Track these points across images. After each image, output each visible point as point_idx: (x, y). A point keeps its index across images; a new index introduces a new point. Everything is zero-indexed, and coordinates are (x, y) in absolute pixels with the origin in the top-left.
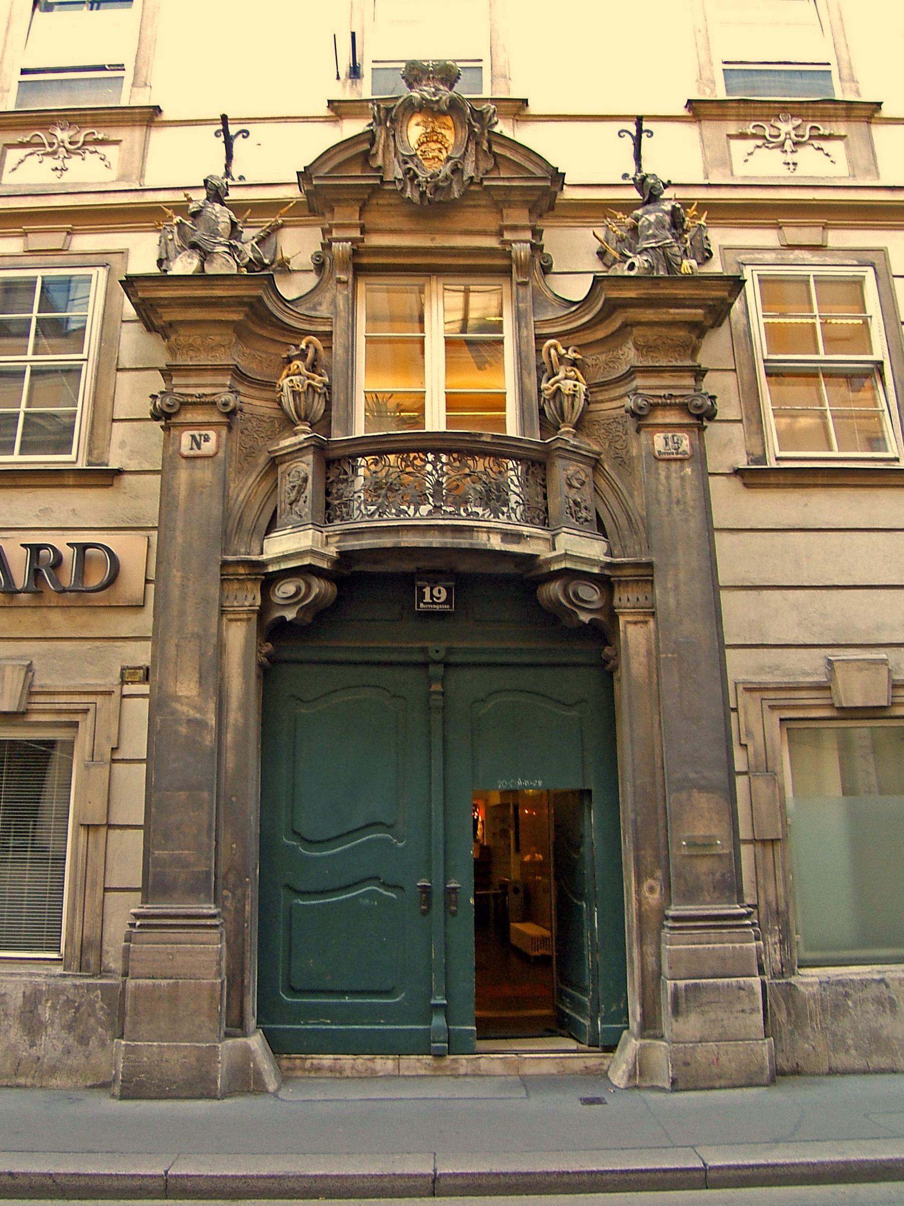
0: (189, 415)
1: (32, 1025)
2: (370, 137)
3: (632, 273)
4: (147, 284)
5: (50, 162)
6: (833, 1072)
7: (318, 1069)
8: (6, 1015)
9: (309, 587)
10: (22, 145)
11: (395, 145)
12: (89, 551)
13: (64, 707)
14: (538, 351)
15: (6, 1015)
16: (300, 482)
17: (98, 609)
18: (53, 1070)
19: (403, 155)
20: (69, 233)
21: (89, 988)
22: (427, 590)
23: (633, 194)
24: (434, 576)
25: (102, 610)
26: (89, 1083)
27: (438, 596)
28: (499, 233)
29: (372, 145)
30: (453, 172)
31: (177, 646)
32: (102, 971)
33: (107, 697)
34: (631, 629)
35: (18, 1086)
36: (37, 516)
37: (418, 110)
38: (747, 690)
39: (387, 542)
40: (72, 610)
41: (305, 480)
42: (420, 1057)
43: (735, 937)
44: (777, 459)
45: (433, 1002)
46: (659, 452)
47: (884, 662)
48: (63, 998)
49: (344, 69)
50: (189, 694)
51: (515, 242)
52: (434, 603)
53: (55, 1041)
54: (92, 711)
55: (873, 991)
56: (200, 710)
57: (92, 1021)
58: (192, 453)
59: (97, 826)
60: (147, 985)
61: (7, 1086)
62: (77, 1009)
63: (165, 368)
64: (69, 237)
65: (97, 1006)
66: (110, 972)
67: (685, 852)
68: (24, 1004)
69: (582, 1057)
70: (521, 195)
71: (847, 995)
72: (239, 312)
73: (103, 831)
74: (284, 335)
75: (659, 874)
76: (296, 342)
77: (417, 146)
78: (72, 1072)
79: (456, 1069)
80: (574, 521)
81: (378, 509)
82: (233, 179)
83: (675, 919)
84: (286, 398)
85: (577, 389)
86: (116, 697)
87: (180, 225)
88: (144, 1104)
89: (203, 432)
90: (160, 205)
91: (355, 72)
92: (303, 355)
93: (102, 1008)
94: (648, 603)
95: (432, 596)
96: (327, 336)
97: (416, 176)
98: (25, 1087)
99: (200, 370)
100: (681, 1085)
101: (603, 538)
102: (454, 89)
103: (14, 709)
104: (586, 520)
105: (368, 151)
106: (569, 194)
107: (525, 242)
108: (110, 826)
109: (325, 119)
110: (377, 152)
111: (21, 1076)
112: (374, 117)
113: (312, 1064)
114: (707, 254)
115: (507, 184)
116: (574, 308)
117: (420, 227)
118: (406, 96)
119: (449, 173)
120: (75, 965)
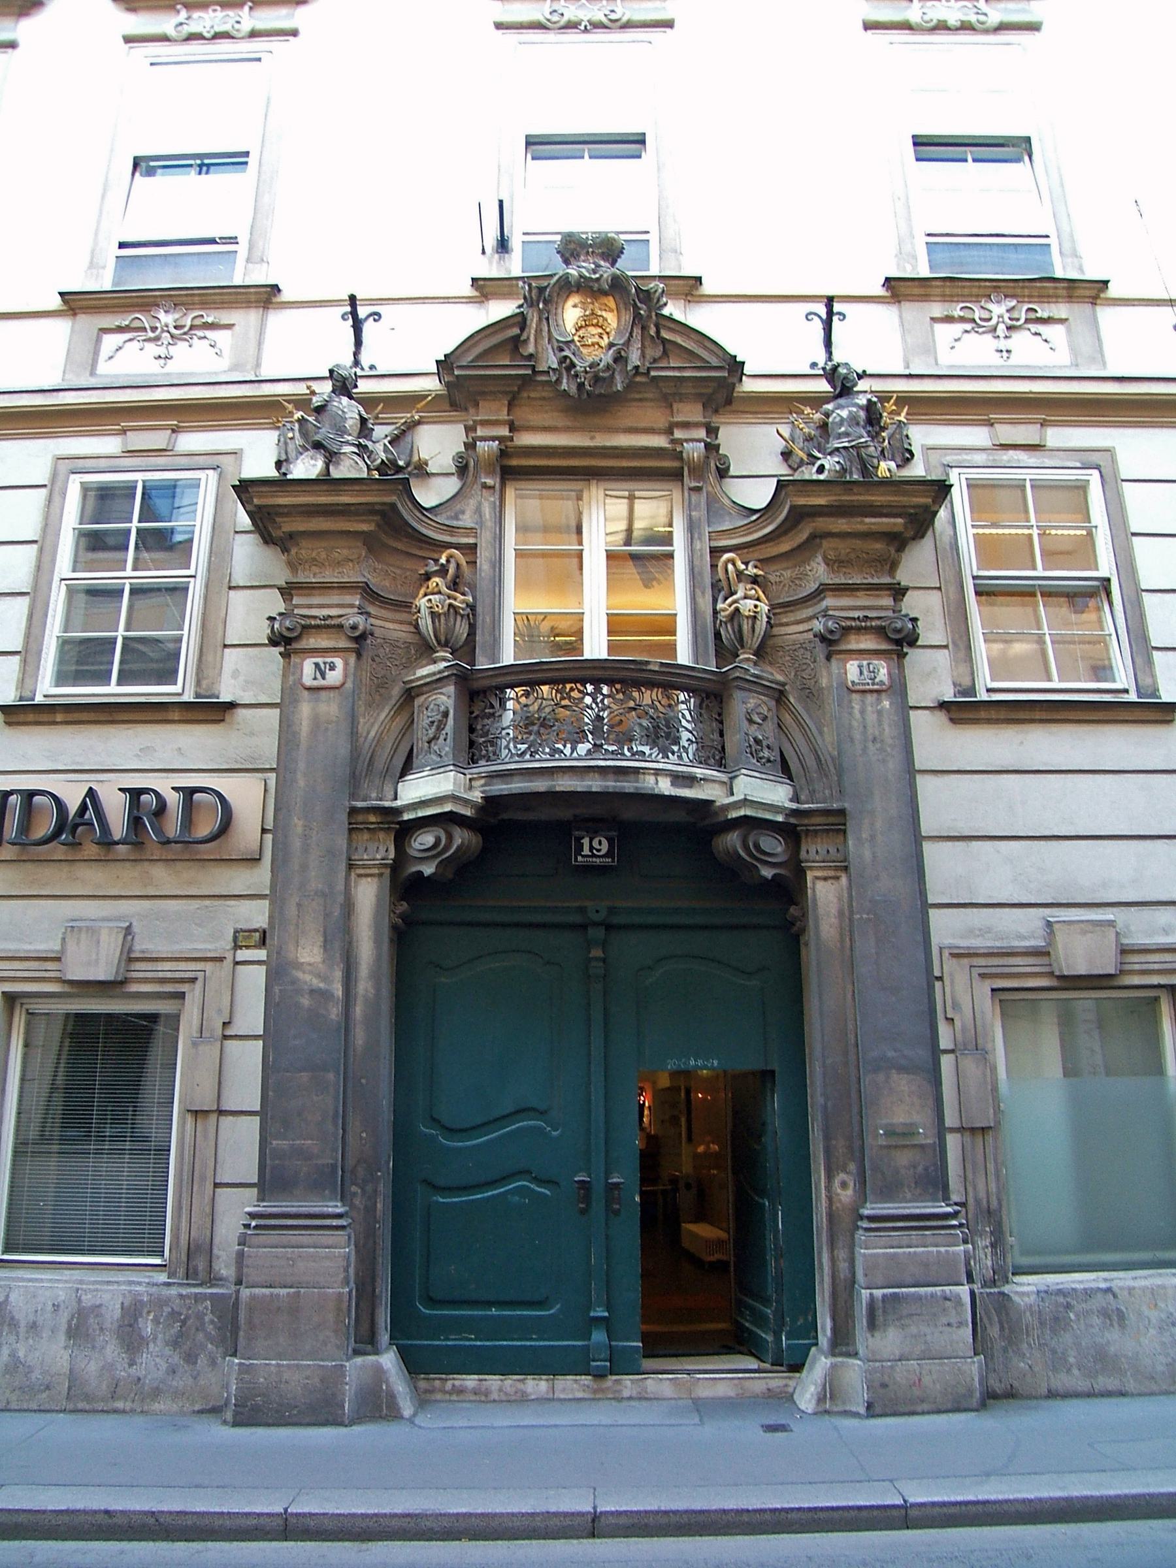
0: (312, 641)
1: (131, 1339)
2: (520, 320)
3: (822, 477)
4: (264, 489)
5: (152, 349)
6: (1052, 1395)
7: (461, 1391)
8: (101, 1329)
9: (450, 837)
10: (120, 329)
11: (549, 330)
12: (197, 796)
13: (169, 975)
15: (101, 1329)
16: (439, 717)
17: (207, 863)
18: (156, 1393)
19: (558, 341)
20: (174, 431)
21: (198, 1298)
22: (586, 842)
23: (823, 386)
24: (594, 825)
25: (212, 863)
26: (196, 1408)
28: (669, 431)
30: (616, 360)
31: (299, 905)
32: (212, 1279)
33: (218, 964)
34: (820, 885)
35: (116, 1411)
36: (137, 756)
38: (953, 955)
39: (540, 785)
40: (178, 863)
41: (446, 714)
42: (578, 1377)
43: (940, 1239)
44: (988, 690)
45: (592, 1314)
46: (853, 682)
47: (1111, 923)
48: (167, 1310)
49: (491, 242)
50: (313, 960)
51: (687, 441)
52: (594, 856)
53: (158, 1360)
54: (201, 980)
55: (1099, 1301)
56: (325, 979)
57: (201, 1335)
58: (315, 683)
60: (264, 1295)
61: (102, 1411)
62: (184, 1322)
63: (284, 585)
65: (207, 1319)
66: (221, 1279)
67: (882, 1142)
68: (123, 1316)
70: (694, 387)
71: (1068, 1306)
72: (369, 522)
73: (213, 1118)
74: (421, 548)
75: (852, 1167)
76: (436, 556)
77: (574, 331)
78: (177, 1394)
79: (620, 1391)
81: (529, 748)
86: (228, 963)
87: (302, 421)
88: (260, 1431)
89: (329, 660)
91: (503, 245)
92: (443, 571)
93: (212, 1322)
94: (840, 856)
95: (591, 848)
97: (573, 365)
98: (124, 1412)
99: (325, 587)
100: (878, 1410)
102: (617, 265)
103: (111, 978)
105: (518, 336)
108: (221, 1112)
109: (469, 300)
110: (528, 338)
111: (119, 1399)
112: (525, 298)
113: (453, 1385)
115: (677, 374)
116: (754, 517)
117: (560, 424)
118: (561, 273)
119: (611, 362)
120: (181, 1271)
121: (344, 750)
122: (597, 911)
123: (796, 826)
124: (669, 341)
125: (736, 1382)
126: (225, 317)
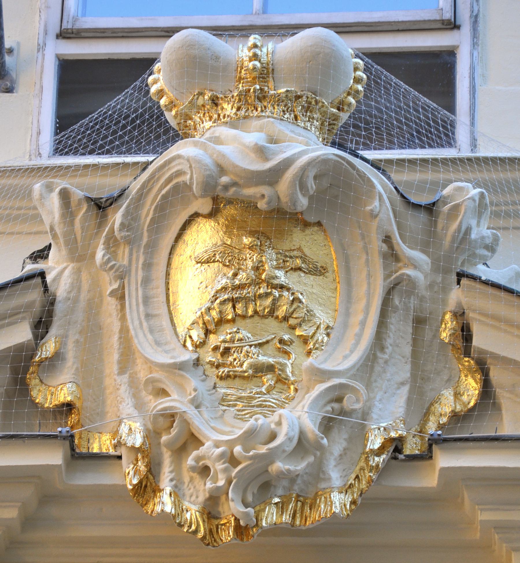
11: (124, 331)
19: (152, 365)
29: (42, 325)
30: (327, 425)
37: (204, 205)
77: (197, 334)
97: (192, 440)
119: (311, 427)
121: (139, 417)
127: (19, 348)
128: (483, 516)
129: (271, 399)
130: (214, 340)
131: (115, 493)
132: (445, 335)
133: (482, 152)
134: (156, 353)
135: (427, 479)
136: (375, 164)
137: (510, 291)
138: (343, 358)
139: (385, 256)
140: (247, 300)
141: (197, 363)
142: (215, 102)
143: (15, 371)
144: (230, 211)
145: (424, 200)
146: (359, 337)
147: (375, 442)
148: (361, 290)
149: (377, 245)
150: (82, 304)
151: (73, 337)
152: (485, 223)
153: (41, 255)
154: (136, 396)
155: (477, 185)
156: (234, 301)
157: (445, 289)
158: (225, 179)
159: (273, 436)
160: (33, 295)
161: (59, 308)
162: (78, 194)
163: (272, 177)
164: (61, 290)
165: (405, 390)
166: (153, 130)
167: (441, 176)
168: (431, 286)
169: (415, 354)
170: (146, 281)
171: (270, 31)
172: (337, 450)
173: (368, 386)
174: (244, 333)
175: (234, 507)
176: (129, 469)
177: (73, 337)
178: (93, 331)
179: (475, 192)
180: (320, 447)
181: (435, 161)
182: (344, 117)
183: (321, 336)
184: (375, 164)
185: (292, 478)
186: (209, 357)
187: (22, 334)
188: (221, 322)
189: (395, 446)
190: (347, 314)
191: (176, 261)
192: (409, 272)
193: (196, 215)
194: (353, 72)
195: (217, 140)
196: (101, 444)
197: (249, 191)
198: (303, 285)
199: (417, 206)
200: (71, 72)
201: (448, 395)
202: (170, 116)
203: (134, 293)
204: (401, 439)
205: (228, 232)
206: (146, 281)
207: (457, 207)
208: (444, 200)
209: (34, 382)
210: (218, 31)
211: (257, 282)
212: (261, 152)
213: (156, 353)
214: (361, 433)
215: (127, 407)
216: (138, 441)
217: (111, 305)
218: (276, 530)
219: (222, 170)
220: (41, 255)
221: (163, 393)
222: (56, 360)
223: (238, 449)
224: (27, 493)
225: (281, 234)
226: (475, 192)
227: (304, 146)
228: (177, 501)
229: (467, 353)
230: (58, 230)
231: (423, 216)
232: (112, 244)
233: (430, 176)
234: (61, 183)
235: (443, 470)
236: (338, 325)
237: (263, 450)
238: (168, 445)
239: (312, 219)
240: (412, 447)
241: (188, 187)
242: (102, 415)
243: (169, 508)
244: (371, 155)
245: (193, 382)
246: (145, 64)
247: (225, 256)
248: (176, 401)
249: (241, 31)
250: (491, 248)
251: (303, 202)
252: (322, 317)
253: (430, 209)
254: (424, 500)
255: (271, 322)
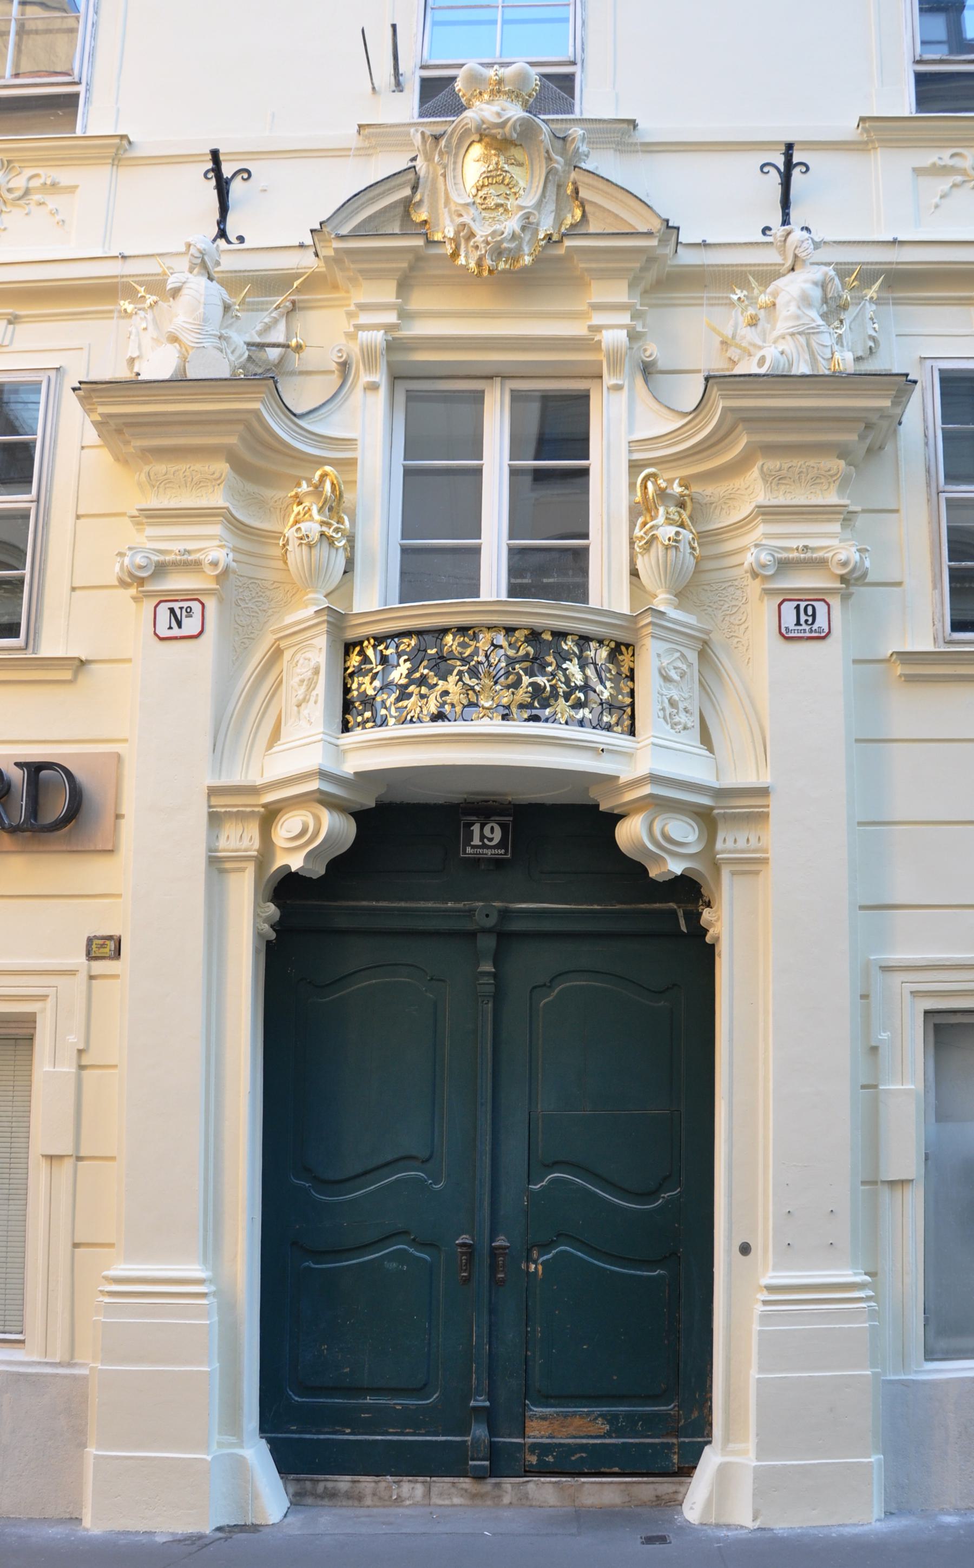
3: (762, 371)
9: (318, 820)
12: (44, 773)
14: (632, 486)
20: (10, 322)
22: (476, 828)
27: (490, 836)
29: (415, 188)
30: (523, 228)
37: (476, 137)
41: (316, 671)
42: (456, 1480)
45: (472, 1403)
46: (787, 628)
52: (484, 846)
59: (61, 1157)
63: (136, 513)
64: (11, 327)
69: (653, 1483)
73: (68, 1164)
76: (308, 475)
77: (474, 191)
80: (668, 727)
82: (229, 242)
83: (771, 1289)
84: (292, 554)
85: (304, 532)
86: (82, 977)
90: (130, 280)
95: (482, 837)
96: (351, 464)
97: (472, 235)
101: (707, 753)
104: (685, 728)
106: (687, 258)
107: (620, 327)
108: (79, 1159)
110: (421, 201)
113: (325, 1488)
114: (872, 344)
119: (518, 230)
122: (487, 916)
123: (712, 808)
124: (591, 202)
125: (623, 1487)
126: (65, 176)
127: (407, 197)
128: (582, 265)
129: (502, 218)
130: (480, 194)
131: (442, 257)
132: (569, 192)
133: (585, 116)
134: (459, 199)
135: (561, 251)
136: (543, 120)
137: (593, 173)
138: (529, 200)
139: (546, 159)
140: (493, 177)
141: (474, 203)
142: (481, 94)
143: (405, 207)
144: (487, 140)
145: (562, 136)
146: (536, 192)
147: (541, 236)
148: (537, 173)
149: (543, 154)
150: (430, 179)
151: (427, 193)
152: (585, 145)
153: (414, 159)
154: (451, 217)
155: (582, 129)
156: (488, 177)
157: (569, 173)
158: (484, 126)
159: (503, 233)
160: (411, 176)
161: (421, 180)
162: (428, 133)
163: (503, 125)
164: (422, 173)
165: (553, 214)
166: (457, 108)
167: (568, 126)
168: (564, 171)
169: (557, 199)
170: (454, 169)
171: (503, 65)
172: (527, 239)
173: (539, 213)
174: (492, 191)
175: (488, 262)
176: (448, 247)
177: (427, 193)
178: (434, 191)
179: (581, 132)
180: (521, 237)
181: (566, 120)
182: (531, 100)
183: (521, 192)
184: (543, 120)
185: (510, 250)
186: (479, 201)
187: (407, 192)
188: (483, 186)
189: (549, 237)
190: (532, 182)
191: (466, 160)
192: (556, 165)
193: (474, 141)
194: (535, 82)
195: (482, 110)
196: (438, 237)
197: (494, 131)
198: (515, 171)
199: (559, 138)
200: (425, 82)
201: (569, 216)
202: (463, 100)
203: (450, 175)
204: (551, 234)
205: (486, 148)
206: (454, 169)
207: (574, 139)
208: (569, 136)
209: (412, 212)
210: (482, 64)
211: (497, 169)
212: (499, 115)
213: (459, 199)
214: (536, 232)
215: (448, 222)
216: (451, 235)
217: (441, 179)
218: (504, 271)
219: (483, 122)
220: (414, 159)
221: (461, 215)
222: (420, 202)
223: (489, 238)
224: (411, 256)
225: (506, 149)
226: (581, 132)
227: (515, 112)
228: (467, 257)
229: (577, 199)
230: (421, 148)
231: (561, 142)
232: (441, 154)
233: (564, 126)
234: (421, 129)
235: (567, 247)
236: (528, 187)
237: (499, 238)
238: (463, 237)
239: (518, 143)
240: (555, 238)
241: (470, 129)
242: (438, 225)
243: (464, 263)
244: (542, 117)
245: (472, 211)
246: (453, 79)
247: (486, 158)
248: (466, 219)
249: (490, 65)
250: (587, 156)
251: (515, 136)
252: (522, 184)
253: (564, 139)
254: (559, 259)
255: (502, 186)
